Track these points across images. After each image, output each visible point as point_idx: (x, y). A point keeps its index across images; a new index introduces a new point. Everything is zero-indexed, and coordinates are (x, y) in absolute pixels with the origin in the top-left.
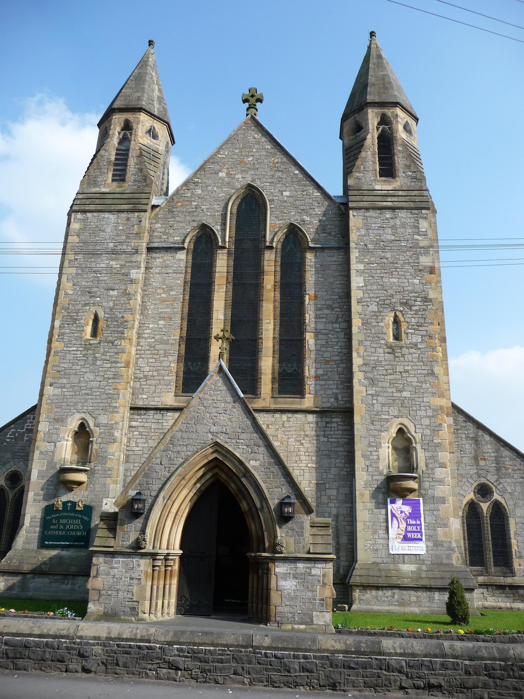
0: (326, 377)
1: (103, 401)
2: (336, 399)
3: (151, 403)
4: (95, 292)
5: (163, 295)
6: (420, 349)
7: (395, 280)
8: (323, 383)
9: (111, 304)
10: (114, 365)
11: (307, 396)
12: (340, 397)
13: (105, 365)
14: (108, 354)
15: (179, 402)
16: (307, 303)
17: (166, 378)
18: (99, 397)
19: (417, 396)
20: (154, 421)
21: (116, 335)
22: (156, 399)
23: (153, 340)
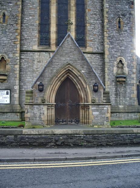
0: (94, 41)
1: (11, 48)
2: (98, 49)
3: (28, 49)
4: (3, 4)
5: (30, 6)
6: (128, 32)
7: (120, 6)
8: (93, 43)
9: (10, 9)
10: (13, 34)
11: (88, 47)
12: (99, 48)
13: (10, 34)
14: (11, 30)
15: (40, 49)
16: (87, 12)
17: (34, 39)
18: (9, 47)
19: (126, 49)
20: (30, 56)
21: (14, 22)
22: (31, 48)
23: (28, 24)
